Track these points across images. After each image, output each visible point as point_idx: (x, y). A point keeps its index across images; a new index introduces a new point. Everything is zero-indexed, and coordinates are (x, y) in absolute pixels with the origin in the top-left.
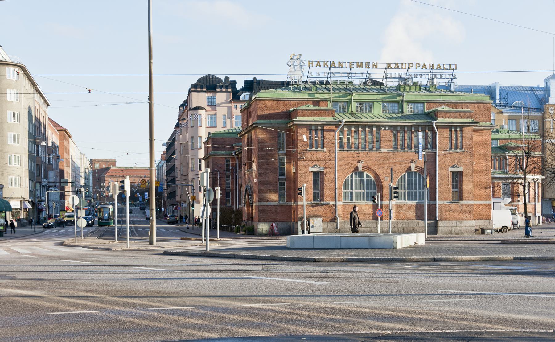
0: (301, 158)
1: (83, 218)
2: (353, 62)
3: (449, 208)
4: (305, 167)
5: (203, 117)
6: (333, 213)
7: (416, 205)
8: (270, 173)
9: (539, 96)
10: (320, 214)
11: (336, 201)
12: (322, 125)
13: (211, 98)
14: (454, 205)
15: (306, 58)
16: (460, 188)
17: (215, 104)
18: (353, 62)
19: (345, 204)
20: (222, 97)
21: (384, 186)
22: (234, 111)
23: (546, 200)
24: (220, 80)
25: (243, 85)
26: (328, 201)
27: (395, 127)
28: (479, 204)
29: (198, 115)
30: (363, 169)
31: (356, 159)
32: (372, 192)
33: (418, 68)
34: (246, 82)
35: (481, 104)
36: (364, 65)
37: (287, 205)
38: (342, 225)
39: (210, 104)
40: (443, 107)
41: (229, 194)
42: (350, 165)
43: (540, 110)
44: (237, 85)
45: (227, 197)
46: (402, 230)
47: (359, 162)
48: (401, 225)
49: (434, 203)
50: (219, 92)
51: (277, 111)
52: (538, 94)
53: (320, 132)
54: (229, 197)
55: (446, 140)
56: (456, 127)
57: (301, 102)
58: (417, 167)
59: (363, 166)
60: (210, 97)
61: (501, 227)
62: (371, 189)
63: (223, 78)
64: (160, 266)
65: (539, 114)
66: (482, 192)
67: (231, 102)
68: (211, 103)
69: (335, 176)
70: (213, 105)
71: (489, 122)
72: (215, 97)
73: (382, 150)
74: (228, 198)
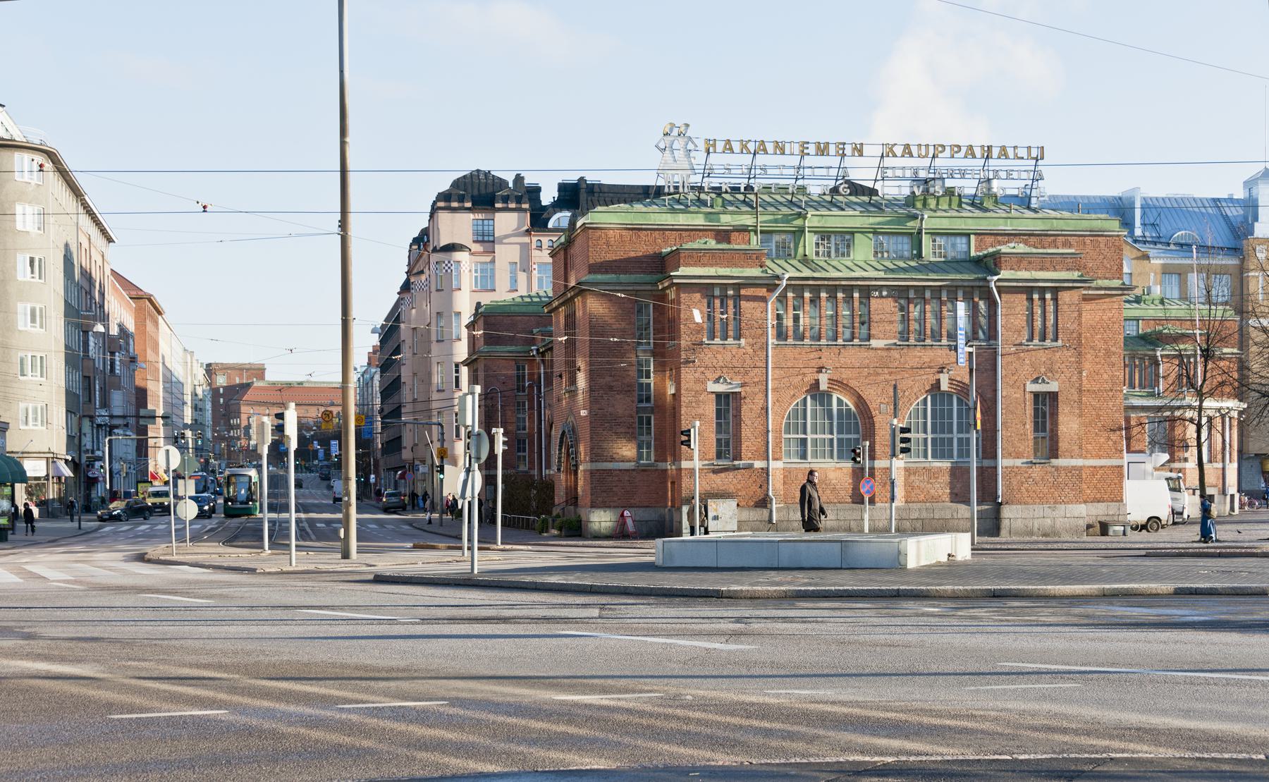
0: (687, 362)
1: (191, 498)
2: (808, 143)
3: (1026, 475)
4: (697, 381)
5: (464, 268)
6: (761, 487)
7: (952, 468)
8: (617, 396)
9: (1232, 219)
10: (731, 489)
11: (768, 460)
12: (737, 287)
13: (483, 225)
14: (1037, 468)
15: (699, 133)
16: (1052, 430)
17: (491, 239)
18: (808, 143)
19: (789, 466)
20: (507, 222)
21: (877, 426)
22: (535, 253)
23: (1249, 458)
24: (502, 183)
25: (556, 195)
26: (750, 458)
27: (902, 291)
28: (1095, 467)
29: (452, 262)
30: (830, 386)
31: (815, 363)
32: (851, 439)
33: (956, 155)
34: (563, 188)
35: (1099, 239)
36: (832, 149)
37: (657, 470)
38: (782, 514)
39: (480, 238)
40: (1012, 245)
41: (524, 443)
42: (800, 377)
43: (1235, 250)
44: (541, 194)
45: (519, 451)
46: (918, 525)
47: (820, 370)
48: (916, 515)
49: (993, 465)
50: (500, 210)
51: (632, 254)
52: (1229, 214)
53: (731, 303)
54: (524, 451)
55: (1020, 321)
56: (1042, 290)
57: (688, 233)
58: (954, 382)
59: (829, 379)
60: (480, 222)
61: (1145, 520)
62: (849, 432)
63: (510, 178)
64: (367, 608)
65: (1232, 261)
66: (1102, 440)
67: (528, 232)
68: (483, 235)
69: (767, 402)
70: (487, 240)
71: (1118, 278)
72: (491, 222)
73: (874, 343)
74: (521, 454)
